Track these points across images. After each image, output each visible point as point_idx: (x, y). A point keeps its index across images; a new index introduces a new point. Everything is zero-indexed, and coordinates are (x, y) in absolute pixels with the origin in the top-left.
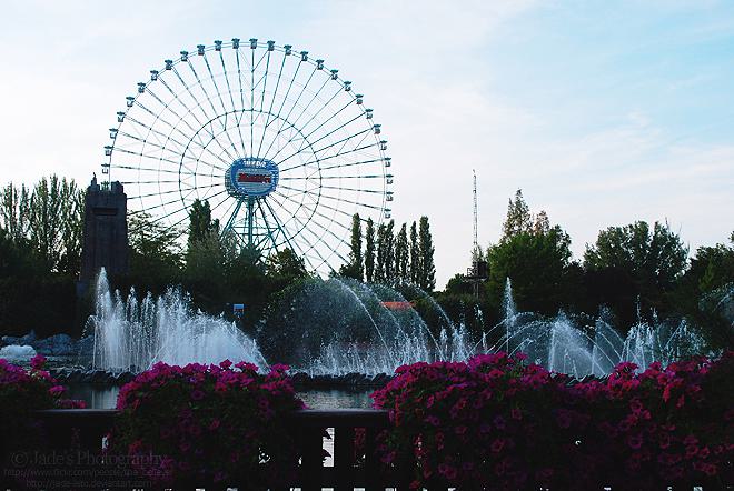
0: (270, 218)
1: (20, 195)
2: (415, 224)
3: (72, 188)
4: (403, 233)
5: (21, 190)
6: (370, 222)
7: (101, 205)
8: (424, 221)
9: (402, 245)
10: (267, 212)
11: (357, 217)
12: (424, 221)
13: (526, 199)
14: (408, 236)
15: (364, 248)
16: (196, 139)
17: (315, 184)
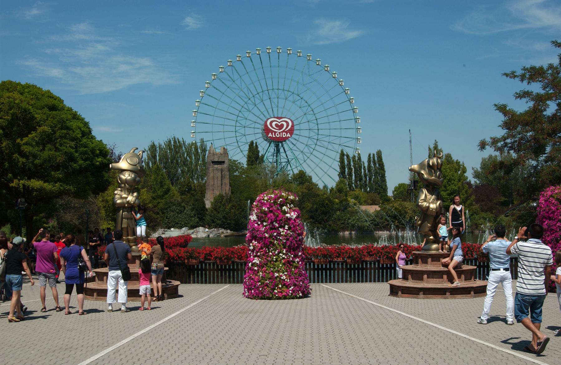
7: (216, 160)
11: (342, 154)
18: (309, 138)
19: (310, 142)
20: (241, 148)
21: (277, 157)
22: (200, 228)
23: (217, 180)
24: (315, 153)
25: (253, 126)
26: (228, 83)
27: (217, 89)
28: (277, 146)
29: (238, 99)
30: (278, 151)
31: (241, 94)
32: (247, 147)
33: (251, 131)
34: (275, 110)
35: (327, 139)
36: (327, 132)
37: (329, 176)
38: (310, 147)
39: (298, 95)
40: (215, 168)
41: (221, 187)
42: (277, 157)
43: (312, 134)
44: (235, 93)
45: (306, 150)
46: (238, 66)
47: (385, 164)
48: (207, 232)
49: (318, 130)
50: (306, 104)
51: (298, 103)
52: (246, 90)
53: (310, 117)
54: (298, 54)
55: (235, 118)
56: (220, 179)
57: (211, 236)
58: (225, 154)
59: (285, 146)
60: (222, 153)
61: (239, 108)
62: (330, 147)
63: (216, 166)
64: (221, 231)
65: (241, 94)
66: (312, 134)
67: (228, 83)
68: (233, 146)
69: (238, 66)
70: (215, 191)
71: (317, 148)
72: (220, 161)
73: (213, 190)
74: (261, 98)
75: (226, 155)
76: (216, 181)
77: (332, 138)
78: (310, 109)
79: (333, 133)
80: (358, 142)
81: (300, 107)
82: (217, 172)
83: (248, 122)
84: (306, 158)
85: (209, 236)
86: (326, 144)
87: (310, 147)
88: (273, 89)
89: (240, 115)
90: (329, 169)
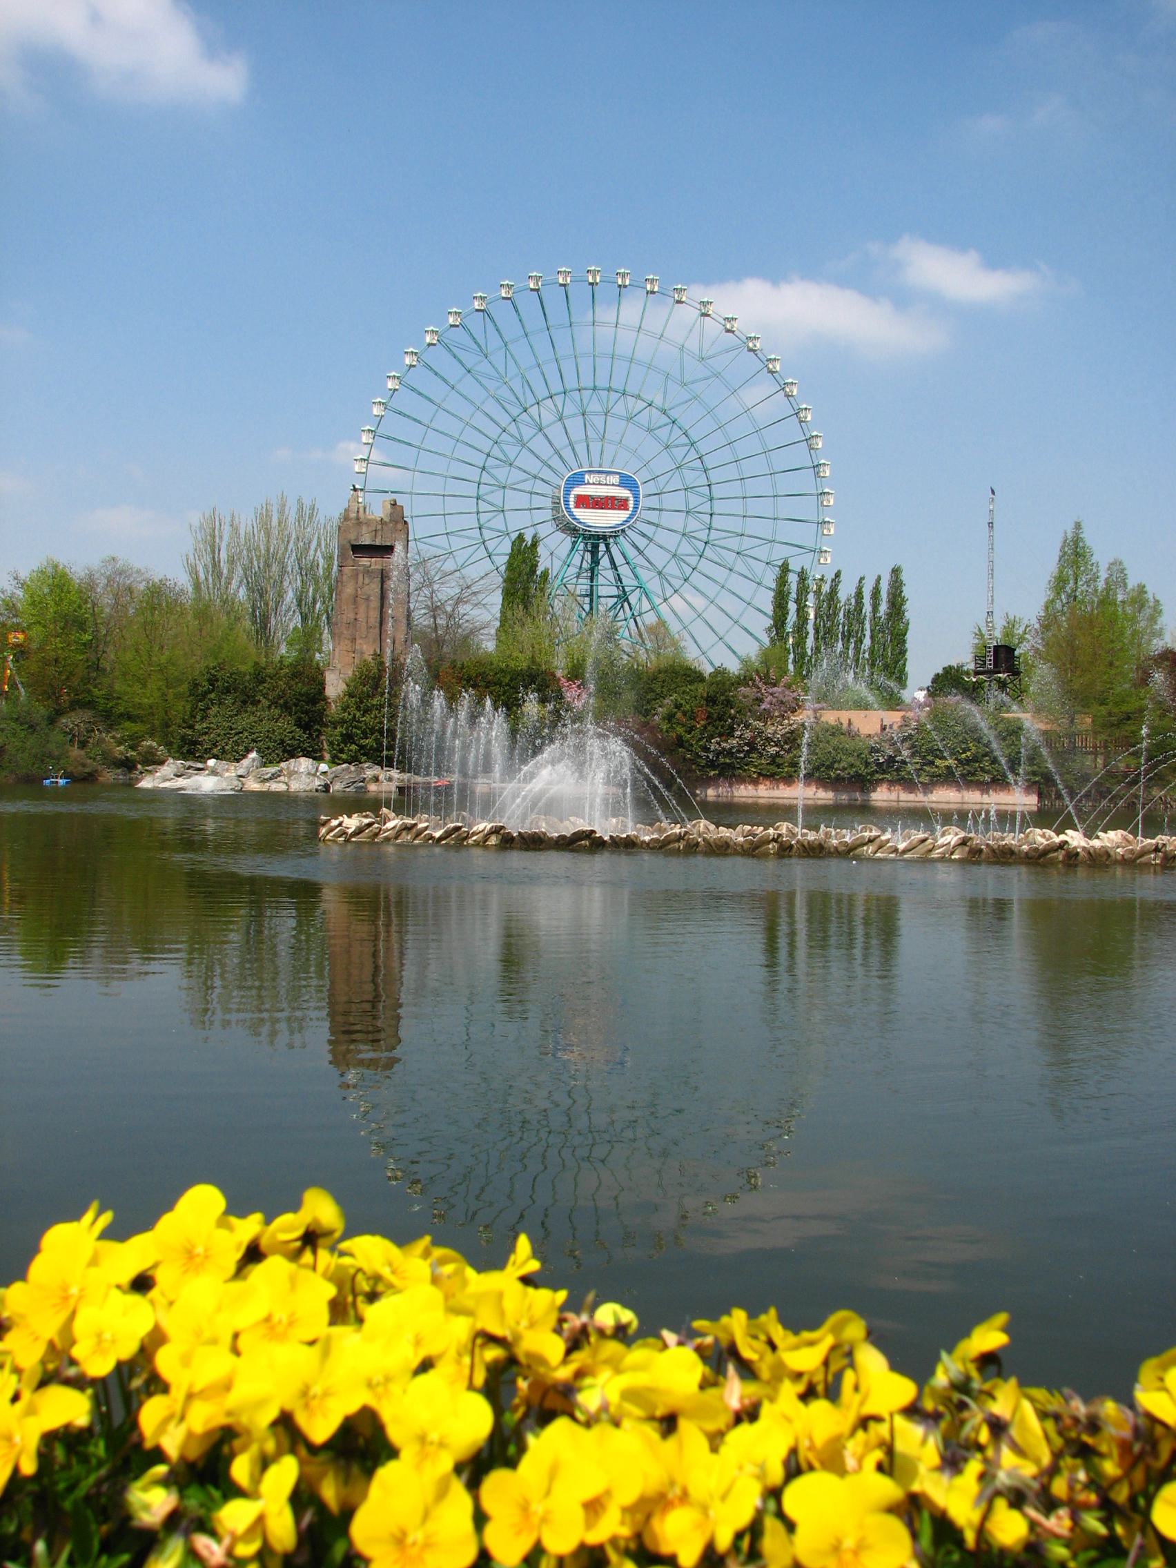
0: (624, 570)
1: (227, 529)
2: (879, 579)
3: (311, 517)
4: (859, 595)
5: (228, 519)
6: (803, 577)
7: (366, 540)
8: (896, 572)
9: (855, 613)
10: (619, 560)
11: (785, 569)
12: (896, 572)
13: (1090, 538)
14: (867, 601)
15: (792, 618)
16: (559, 400)
17: (701, 495)
18: (687, 512)
19: (685, 548)
20: (491, 545)
21: (592, 582)
22: (303, 760)
23: (368, 607)
24: (696, 578)
25: (527, 486)
26: (470, 359)
27: (436, 374)
28: (594, 551)
29: (492, 407)
30: (595, 561)
31: (504, 393)
32: (506, 547)
33: (522, 500)
34: (595, 447)
35: (734, 543)
36: (735, 525)
37: (745, 629)
38: (685, 562)
39: (664, 412)
40: (361, 568)
41: (377, 630)
42: (592, 582)
43: (693, 525)
44: (485, 388)
45: (672, 569)
46: (503, 313)
47: (1056, 554)
48: (325, 773)
49: (711, 515)
50: (684, 440)
51: (663, 433)
52: (517, 385)
53: (694, 477)
54: (676, 296)
55: (479, 459)
56: (375, 603)
57: (337, 787)
58: (396, 522)
59: (614, 550)
60: (387, 519)
61: (494, 432)
62: (740, 566)
63: (365, 561)
64: (369, 773)
65: (504, 393)
66: (694, 500)
67: (470, 359)
68: (468, 537)
69: (503, 313)
70: (358, 641)
71: (704, 566)
72: (378, 543)
73: (354, 640)
74: (558, 410)
75: (400, 526)
76: (362, 609)
77: (747, 543)
78: (693, 455)
79: (753, 527)
80: (822, 561)
81: (667, 447)
82: (367, 581)
83: (516, 475)
84: (669, 591)
85: (327, 788)
86: (730, 557)
87: (685, 562)
88: (595, 388)
89: (496, 452)
90: (745, 609)
